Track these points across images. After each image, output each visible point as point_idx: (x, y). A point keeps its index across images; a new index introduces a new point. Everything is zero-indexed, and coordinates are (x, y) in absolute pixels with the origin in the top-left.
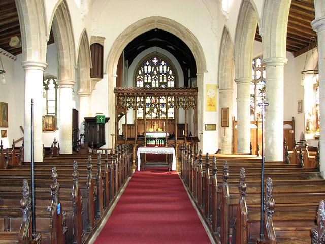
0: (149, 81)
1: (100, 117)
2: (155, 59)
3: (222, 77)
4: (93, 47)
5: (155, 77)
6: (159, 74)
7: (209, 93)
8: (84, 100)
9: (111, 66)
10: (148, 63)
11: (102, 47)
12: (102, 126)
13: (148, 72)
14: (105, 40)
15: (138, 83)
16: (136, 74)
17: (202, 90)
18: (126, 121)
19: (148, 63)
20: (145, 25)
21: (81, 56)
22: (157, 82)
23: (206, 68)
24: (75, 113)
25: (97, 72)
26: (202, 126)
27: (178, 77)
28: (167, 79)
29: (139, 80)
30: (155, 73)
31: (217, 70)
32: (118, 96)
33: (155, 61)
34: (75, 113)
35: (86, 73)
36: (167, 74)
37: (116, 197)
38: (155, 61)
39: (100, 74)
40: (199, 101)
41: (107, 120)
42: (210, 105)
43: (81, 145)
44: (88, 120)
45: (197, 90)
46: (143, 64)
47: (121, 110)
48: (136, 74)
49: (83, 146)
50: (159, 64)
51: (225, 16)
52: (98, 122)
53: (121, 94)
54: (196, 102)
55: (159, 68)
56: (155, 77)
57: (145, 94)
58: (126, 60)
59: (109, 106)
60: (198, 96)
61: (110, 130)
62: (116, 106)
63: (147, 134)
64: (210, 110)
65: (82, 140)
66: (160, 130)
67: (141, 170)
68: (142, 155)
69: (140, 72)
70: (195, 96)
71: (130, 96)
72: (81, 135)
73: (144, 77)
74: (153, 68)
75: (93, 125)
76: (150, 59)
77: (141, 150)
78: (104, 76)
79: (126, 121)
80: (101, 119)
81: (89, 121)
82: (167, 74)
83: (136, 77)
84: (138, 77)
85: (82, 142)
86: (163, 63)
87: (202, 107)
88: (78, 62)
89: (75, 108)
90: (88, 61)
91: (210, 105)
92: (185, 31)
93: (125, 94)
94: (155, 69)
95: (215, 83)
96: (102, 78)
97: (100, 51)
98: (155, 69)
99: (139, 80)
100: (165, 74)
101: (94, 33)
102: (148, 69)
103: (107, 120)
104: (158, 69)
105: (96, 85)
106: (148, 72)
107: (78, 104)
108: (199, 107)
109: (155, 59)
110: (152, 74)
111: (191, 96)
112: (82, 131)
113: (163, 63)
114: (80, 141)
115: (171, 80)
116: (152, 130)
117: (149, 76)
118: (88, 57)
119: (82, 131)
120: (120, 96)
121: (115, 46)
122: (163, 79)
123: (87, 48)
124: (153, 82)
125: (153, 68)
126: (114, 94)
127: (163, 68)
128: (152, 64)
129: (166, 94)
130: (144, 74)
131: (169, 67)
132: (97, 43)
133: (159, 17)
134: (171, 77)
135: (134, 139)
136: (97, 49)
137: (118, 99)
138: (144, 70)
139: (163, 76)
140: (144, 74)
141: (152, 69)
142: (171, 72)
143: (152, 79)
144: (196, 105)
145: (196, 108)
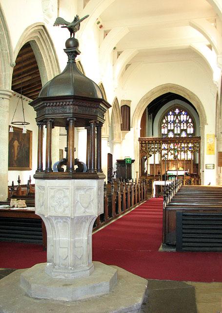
0: (172, 128)
1: (128, 159)
2: (177, 110)
3: (218, 129)
4: (123, 108)
5: (177, 125)
6: (180, 122)
7: (208, 141)
8: (117, 147)
9: (136, 121)
10: (171, 113)
11: (129, 108)
12: (129, 166)
13: (171, 121)
14: (131, 103)
15: (163, 130)
16: (161, 122)
17: (204, 138)
18: (154, 162)
19: (171, 113)
20: (161, 90)
21: (114, 116)
22: (179, 129)
23: (206, 122)
24: (110, 156)
25: (126, 126)
26: (203, 164)
27: (196, 125)
28: (187, 126)
29: (164, 128)
30: (177, 121)
31: (215, 123)
32: (141, 143)
33: (177, 111)
34: (110, 156)
35: (118, 127)
36: (187, 122)
37: (131, 209)
38: (177, 111)
39: (128, 127)
40: (202, 147)
41: (133, 161)
42: (210, 150)
43: (114, 179)
44: (119, 162)
45: (200, 138)
46: (167, 114)
47: (144, 154)
48: (161, 122)
49: (116, 180)
50: (180, 114)
51: (216, 85)
52: (126, 163)
53: (144, 142)
54: (199, 147)
55: (180, 117)
56: (177, 125)
57: (161, 142)
58: (149, 114)
59: (135, 151)
60: (201, 143)
61: (135, 169)
62: (140, 151)
63: (168, 172)
64: (210, 154)
65: (115, 176)
66: (181, 169)
67: (156, 197)
68: (158, 187)
69: (164, 121)
70: (199, 143)
71: (157, 143)
72: (114, 172)
73: (168, 125)
74: (175, 117)
75: (123, 165)
76: (173, 110)
77: (155, 183)
78: (131, 129)
79: (154, 162)
80: (129, 160)
81: (121, 163)
82: (187, 122)
83: (161, 125)
84: (162, 125)
85: (115, 177)
86: (183, 113)
87: (204, 151)
88: (112, 119)
89: (110, 153)
90: (119, 118)
91: (210, 150)
92: (190, 94)
93: (154, 142)
94: (177, 118)
95: (214, 133)
96: (130, 130)
97: (128, 111)
98: (177, 118)
99: (164, 128)
100: (185, 122)
101: (123, 98)
102: (171, 118)
103: (133, 161)
104: (179, 119)
105: (125, 136)
106: (171, 121)
107: (112, 149)
108: (201, 152)
109: (177, 110)
110: (174, 122)
111: (195, 143)
112: (115, 169)
113: (183, 113)
114: (113, 176)
115: (190, 127)
116: (174, 168)
117: (172, 124)
118: (119, 116)
119: (115, 169)
120: (143, 143)
121: (138, 107)
122: (184, 127)
123: (118, 110)
124: (176, 129)
125: (175, 117)
126: (138, 142)
127: (183, 117)
128: (174, 114)
129: (177, 141)
130: (167, 122)
131: (188, 116)
132: (127, 106)
133: (171, 84)
134: (190, 124)
135: (153, 176)
136: (125, 110)
137: (142, 146)
138: (167, 118)
139: (184, 124)
140: (167, 122)
141: (174, 118)
142: (190, 121)
143: (174, 127)
144: (200, 150)
145: (199, 152)
